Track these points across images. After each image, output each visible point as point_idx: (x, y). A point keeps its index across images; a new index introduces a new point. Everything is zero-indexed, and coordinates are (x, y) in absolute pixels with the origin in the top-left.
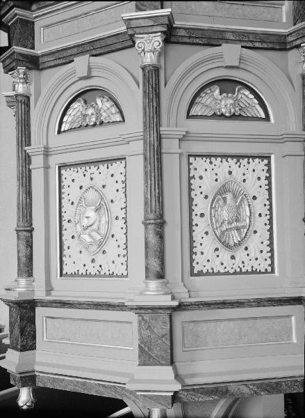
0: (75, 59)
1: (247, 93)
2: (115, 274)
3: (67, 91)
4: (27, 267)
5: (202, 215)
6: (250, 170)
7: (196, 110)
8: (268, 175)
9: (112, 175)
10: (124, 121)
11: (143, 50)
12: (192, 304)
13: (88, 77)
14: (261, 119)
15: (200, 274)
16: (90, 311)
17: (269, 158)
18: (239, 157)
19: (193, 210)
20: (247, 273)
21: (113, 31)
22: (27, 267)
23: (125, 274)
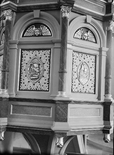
0: (34, 11)
1: (46, 28)
2: (43, 90)
6: (43, 54)
8: (50, 56)
14: (50, 36)
15: (22, 90)
16: (75, 104)
17: (50, 49)
18: (39, 50)
19: (22, 68)
20: (39, 91)
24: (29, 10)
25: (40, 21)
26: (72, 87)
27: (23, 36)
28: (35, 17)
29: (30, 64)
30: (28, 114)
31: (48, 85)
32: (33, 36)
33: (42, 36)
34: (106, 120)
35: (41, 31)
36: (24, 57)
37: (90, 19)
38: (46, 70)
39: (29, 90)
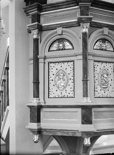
3: (52, 38)
4: (36, 95)
5: (52, 80)
7: (52, 49)
9: (69, 66)
10: (73, 49)
11: (83, 28)
12: (34, 106)
13: (62, 34)
21: (95, 21)
22: (36, 95)
23: (73, 96)
24: (100, 26)
25: (63, 36)
26: (94, 93)
27: (49, 51)
28: (58, 34)
29: (101, 75)
30: (106, 118)
31: (74, 92)
32: (57, 50)
33: (65, 49)
34: (92, 122)
35: (64, 46)
36: (95, 67)
37: (106, 31)
38: (51, 80)
39: (101, 98)
